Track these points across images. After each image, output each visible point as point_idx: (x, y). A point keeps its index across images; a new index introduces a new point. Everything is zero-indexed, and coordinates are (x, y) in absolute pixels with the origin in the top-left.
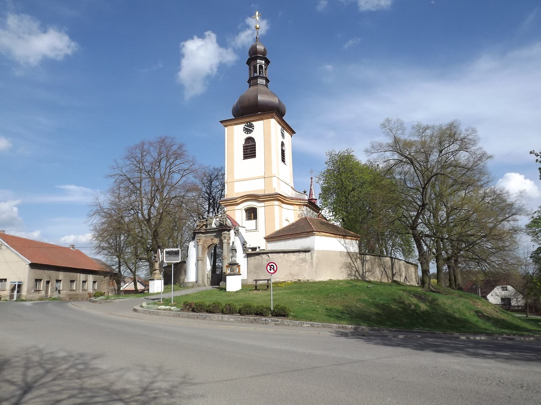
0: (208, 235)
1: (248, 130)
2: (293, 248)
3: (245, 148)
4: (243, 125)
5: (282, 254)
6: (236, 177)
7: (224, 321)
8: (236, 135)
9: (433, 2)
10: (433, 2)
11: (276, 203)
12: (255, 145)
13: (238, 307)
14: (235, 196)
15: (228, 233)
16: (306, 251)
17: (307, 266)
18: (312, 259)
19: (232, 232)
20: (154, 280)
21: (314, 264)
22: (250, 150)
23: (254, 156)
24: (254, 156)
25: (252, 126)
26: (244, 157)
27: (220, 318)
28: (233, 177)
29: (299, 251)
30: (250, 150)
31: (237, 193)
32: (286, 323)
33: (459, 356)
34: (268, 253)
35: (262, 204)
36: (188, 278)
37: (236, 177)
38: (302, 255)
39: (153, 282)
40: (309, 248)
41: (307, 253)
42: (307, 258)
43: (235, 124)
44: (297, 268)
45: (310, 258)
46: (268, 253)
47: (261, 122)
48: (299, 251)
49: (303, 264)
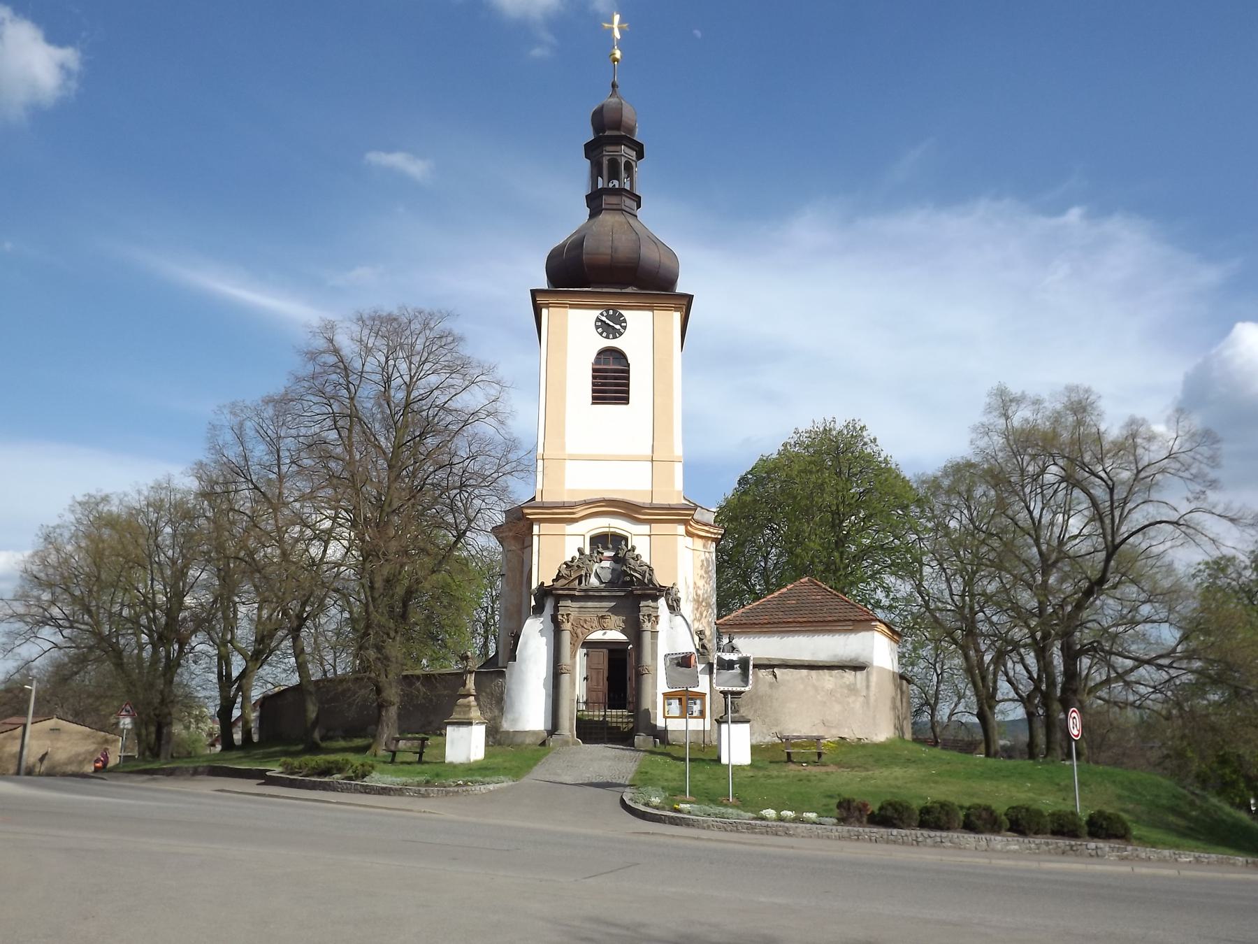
0: (590, 604)
1: (611, 326)
2: (806, 657)
3: (599, 375)
4: (597, 313)
5: (804, 672)
6: (570, 449)
7: (994, 850)
8: (577, 330)
9: (698, 33)
10: (698, 33)
11: (681, 529)
12: (628, 372)
13: (874, 807)
14: (566, 498)
15: (652, 604)
16: (858, 667)
17: (857, 703)
18: (868, 687)
19: (662, 602)
20: (470, 724)
21: (872, 698)
22: (611, 382)
23: (625, 400)
24: (625, 400)
25: (620, 320)
26: (594, 398)
27: (983, 843)
28: (563, 447)
29: (842, 667)
30: (611, 382)
31: (572, 491)
32: (1143, 855)
33: (597, 920)
34: (773, 666)
35: (645, 529)
36: (515, 721)
37: (570, 449)
38: (849, 676)
39: (463, 730)
40: (861, 660)
41: (858, 673)
42: (859, 686)
43: (573, 306)
44: (837, 708)
45: (864, 684)
46: (773, 666)
47: (646, 315)
48: (842, 667)
49: (851, 700)
